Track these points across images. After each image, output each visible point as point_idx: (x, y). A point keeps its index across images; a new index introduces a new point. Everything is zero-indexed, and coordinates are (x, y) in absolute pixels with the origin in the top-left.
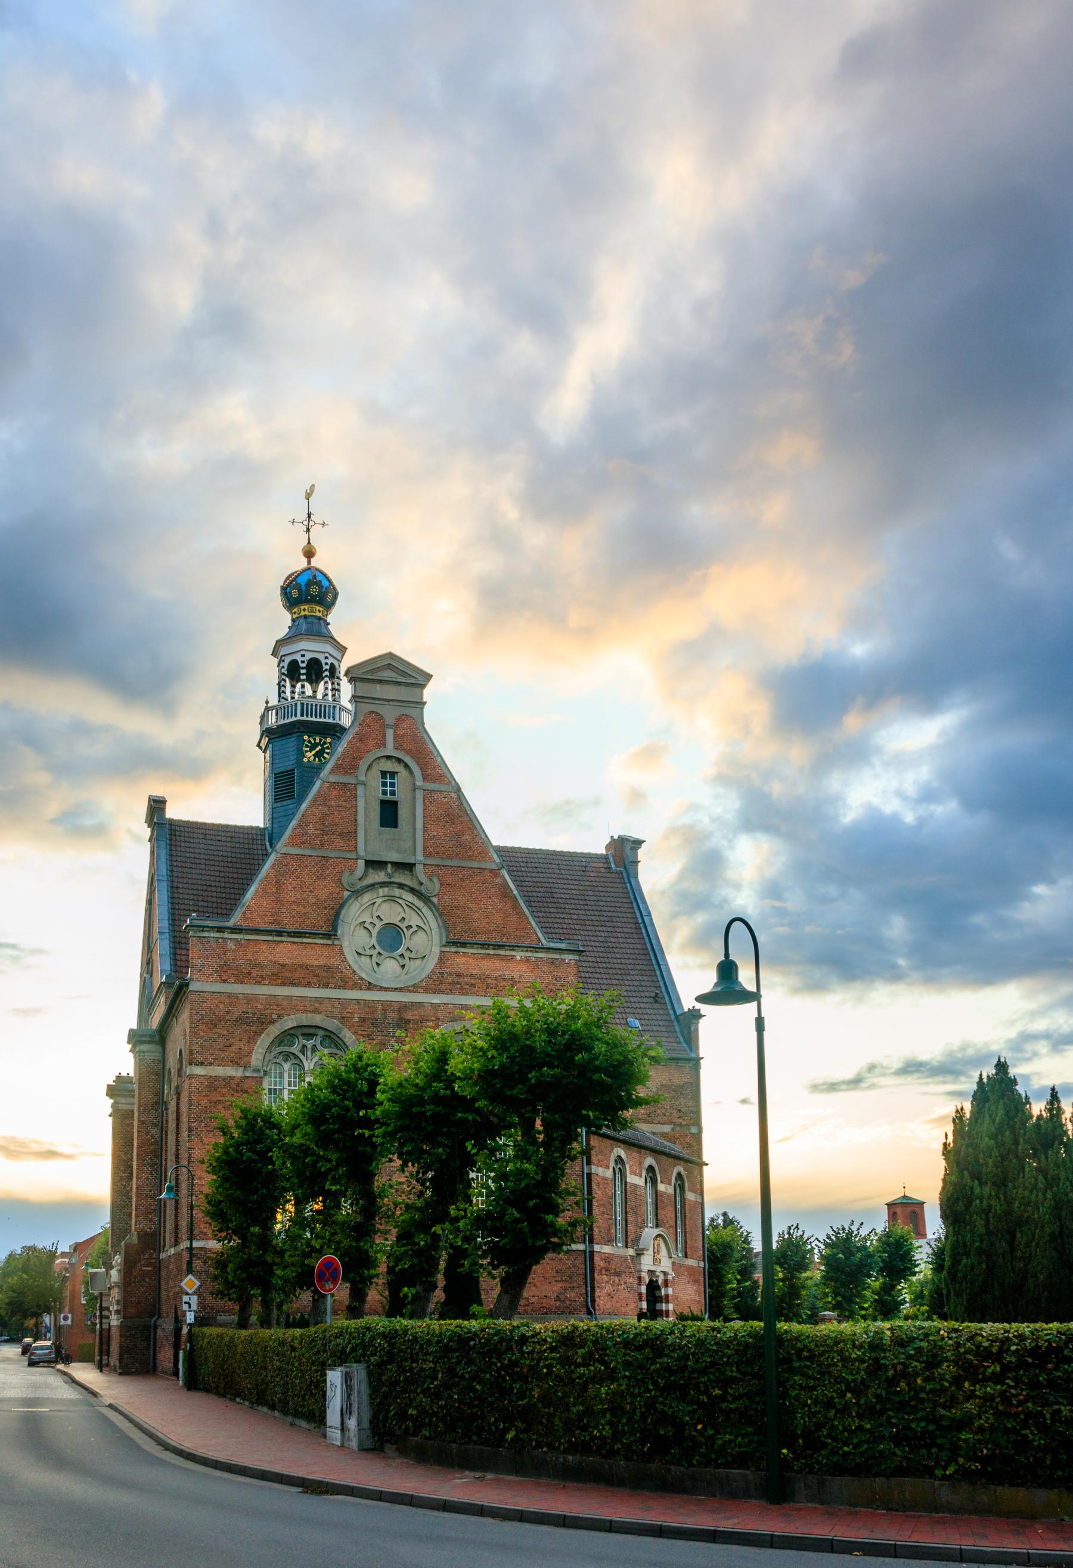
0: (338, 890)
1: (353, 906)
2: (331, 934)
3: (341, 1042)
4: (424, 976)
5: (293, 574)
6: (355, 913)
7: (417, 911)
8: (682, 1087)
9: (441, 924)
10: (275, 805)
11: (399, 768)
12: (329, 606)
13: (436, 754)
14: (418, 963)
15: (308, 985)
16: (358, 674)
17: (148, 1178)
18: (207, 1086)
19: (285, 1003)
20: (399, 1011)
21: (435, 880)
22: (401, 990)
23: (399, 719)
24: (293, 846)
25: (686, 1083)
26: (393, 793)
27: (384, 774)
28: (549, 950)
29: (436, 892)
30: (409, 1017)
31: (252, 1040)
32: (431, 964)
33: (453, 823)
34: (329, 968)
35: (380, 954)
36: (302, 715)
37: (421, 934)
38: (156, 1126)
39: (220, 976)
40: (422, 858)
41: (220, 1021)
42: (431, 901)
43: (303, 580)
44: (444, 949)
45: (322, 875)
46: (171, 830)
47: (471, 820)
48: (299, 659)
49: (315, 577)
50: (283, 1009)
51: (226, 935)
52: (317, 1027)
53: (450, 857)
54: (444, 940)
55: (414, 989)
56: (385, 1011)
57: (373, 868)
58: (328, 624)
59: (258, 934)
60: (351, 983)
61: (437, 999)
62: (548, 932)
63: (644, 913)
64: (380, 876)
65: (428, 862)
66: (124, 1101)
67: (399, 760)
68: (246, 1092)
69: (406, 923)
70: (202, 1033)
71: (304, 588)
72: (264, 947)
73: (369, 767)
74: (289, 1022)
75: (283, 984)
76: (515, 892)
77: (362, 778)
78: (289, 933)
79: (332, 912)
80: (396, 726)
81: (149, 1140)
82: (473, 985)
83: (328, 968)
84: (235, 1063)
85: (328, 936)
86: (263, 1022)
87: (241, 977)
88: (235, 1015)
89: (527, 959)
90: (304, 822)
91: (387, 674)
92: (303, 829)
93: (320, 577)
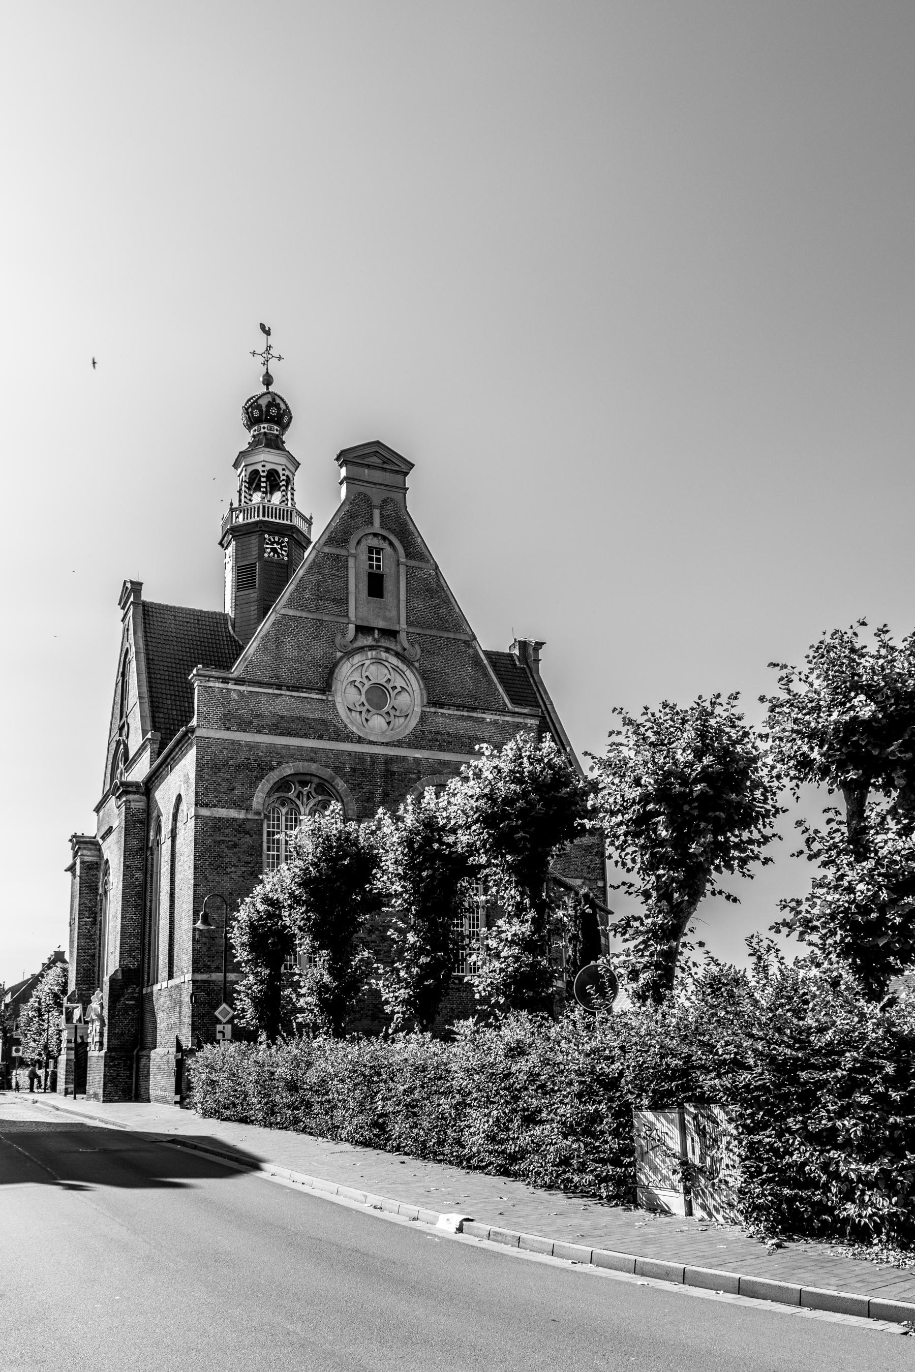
0: (331, 651)
1: (345, 666)
2: (326, 687)
3: (334, 791)
4: (407, 732)
5: (252, 398)
6: (346, 671)
7: (401, 673)
8: (590, 847)
9: (422, 687)
10: (238, 594)
11: (385, 545)
12: (284, 427)
13: (416, 534)
14: (402, 720)
15: (305, 736)
16: (350, 457)
17: (132, 918)
18: (211, 827)
19: (284, 752)
20: (386, 763)
21: (417, 646)
22: (387, 744)
23: (385, 501)
24: (291, 608)
25: (594, 844)
26: (378, 567)
27: (371, 550)
28: (514, 714)
29: (418, 657)
30: (395, 769)
31: (253, 784)
32: (414, 722)
33: (432, 597)
34: (323, 721)
35: (368, 711)
36: (264, 516)
37: (404, 694)
38: (140, 870)
39: (224, 724)
40: (405, 627)
41: (224, 766)
42: (413, 665)
43: (263, 402)
44: (425, 709)
45: (317, 636)
46: (144, 610)
47: (447, 596)
48: (260, 469)
49: (274, 400)
50: (281, 757)
51: (230, 686)
52: (312, 775)
53: (429, 628)
54: (425, 701)
55: (399, 744)
56: (373, 763)
57: (362, 633)
58: (284, 442)
59: (260, 687)
60: (342, 736)
61: (418, 754)
62: (513, 701)
63: (547, 703)
64: (369, 641)
65: (411, 630)
66: (89, 853)
67: (385, 538)
68: (248, 833)
69: (391, 684)
70: (207, 777)
71: (264, 409)
72: (265, 699)
73: (359, 542)
74: (288, 770)
75: (282, 734)
76: (485, 662)
77: (353, 551)
78: (288, 687)
79: (326, 671)
80: (381, 508)
81: (133, 882)
82: (450, 743)
83: (323, 722)
84: (237, 805)
85: (323, 691)
86: (264, 769)
87: (244, 726)
88: (238, 762)
89: (496, 722)
90: (300, 588)
91: (375, 460)
92: (300, 593)
93: (278, 401)
